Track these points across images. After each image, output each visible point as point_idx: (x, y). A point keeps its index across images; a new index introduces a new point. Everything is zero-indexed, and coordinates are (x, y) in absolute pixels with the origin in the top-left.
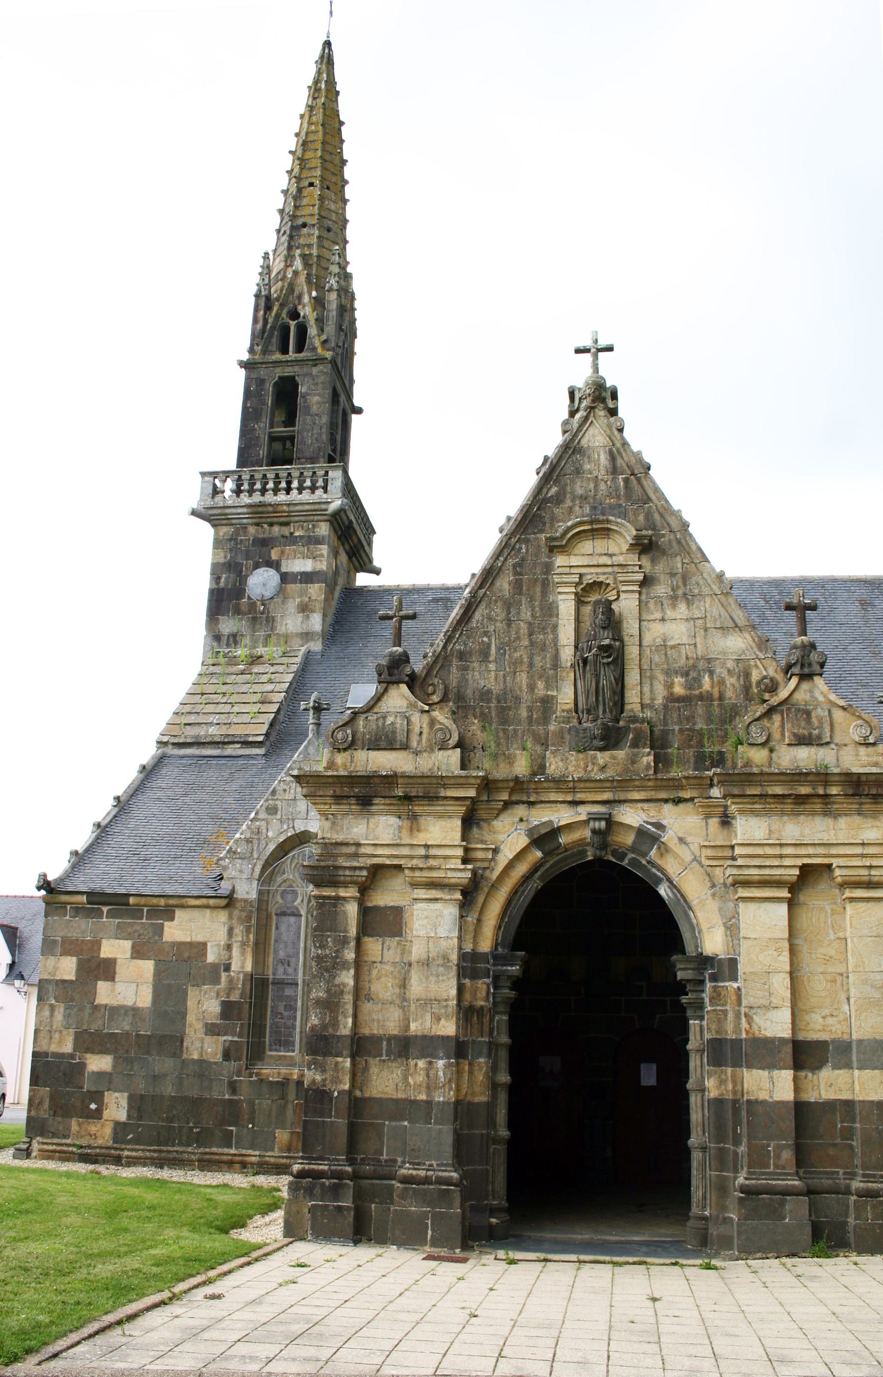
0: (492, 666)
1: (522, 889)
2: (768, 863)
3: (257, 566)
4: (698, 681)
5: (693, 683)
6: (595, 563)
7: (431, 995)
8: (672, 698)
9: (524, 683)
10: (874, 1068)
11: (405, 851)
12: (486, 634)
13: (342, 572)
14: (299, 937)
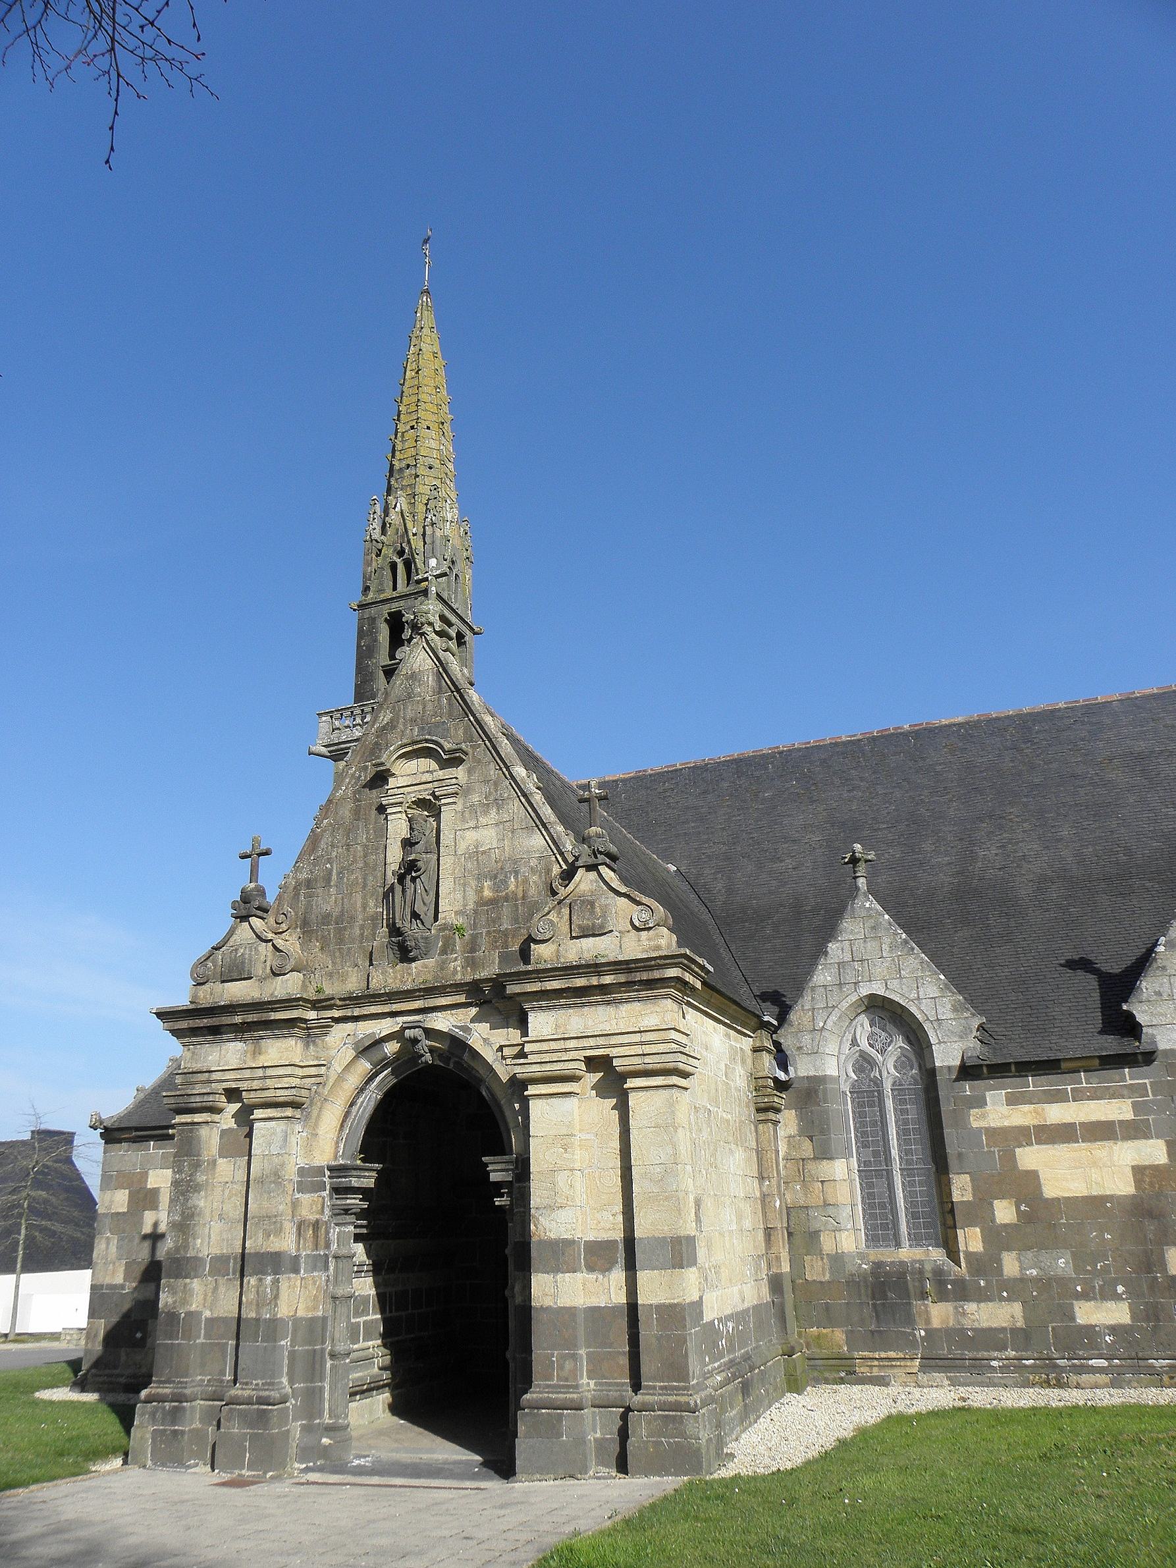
4: (505, 882)
8: (481, 902)
9: (359, 904)
10: (653, 1269)
11: (247, 1074)
12: (329, 861)
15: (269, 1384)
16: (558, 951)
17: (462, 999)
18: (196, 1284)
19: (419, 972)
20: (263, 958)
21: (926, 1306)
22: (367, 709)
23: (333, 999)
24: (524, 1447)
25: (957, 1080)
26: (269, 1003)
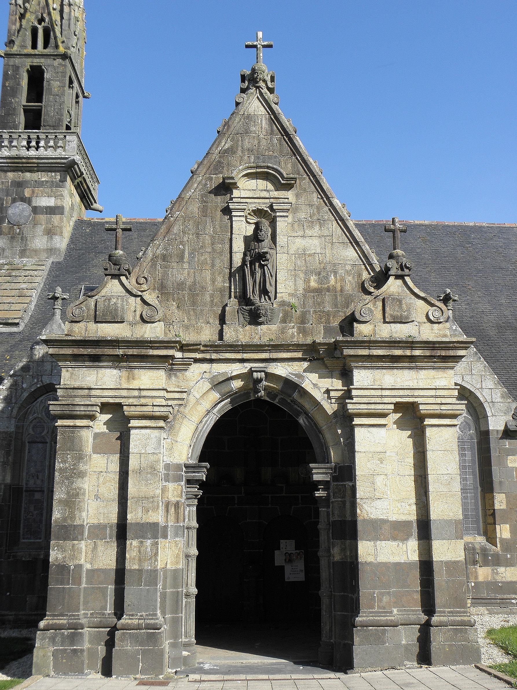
0: (186, 266)
1: (206, 419)
2: (373, 400)
3: (14, 201)
4: (327, 278)
5: (323, 278)
6: (258, 196)
7: (142, 494)
8: (308, 290)
9: (208, 278)
11: (124, 393)
12: (181, 243)
13: (76, 208)
14: (45, 458)
15: (152, 615)
16: (374, 330)
17: (299, 355)
18: (83, 545)
19: (265, 333)
20: (133, 309)
21: (476, 569)
22: (14, 136)
23: (200, 344)
24: (359, 651)
25: (501, 438)
26: (151, 342)
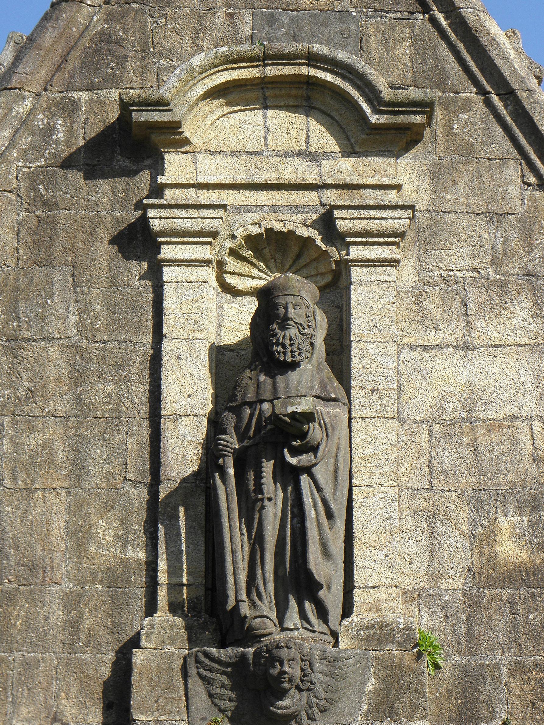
8: (488, 575)
